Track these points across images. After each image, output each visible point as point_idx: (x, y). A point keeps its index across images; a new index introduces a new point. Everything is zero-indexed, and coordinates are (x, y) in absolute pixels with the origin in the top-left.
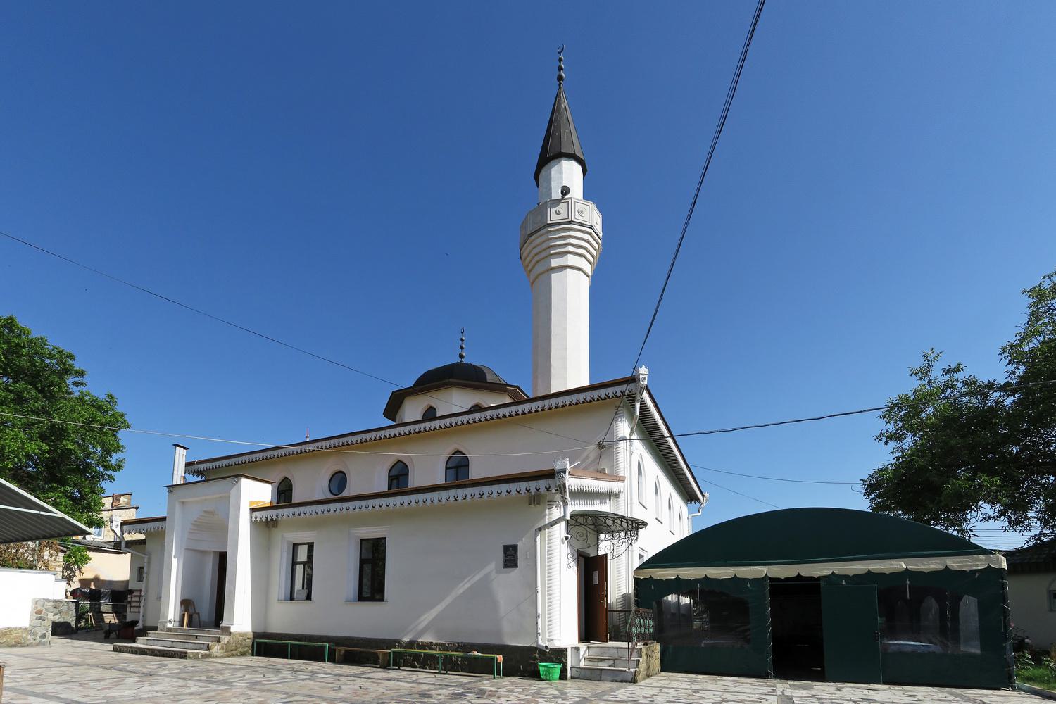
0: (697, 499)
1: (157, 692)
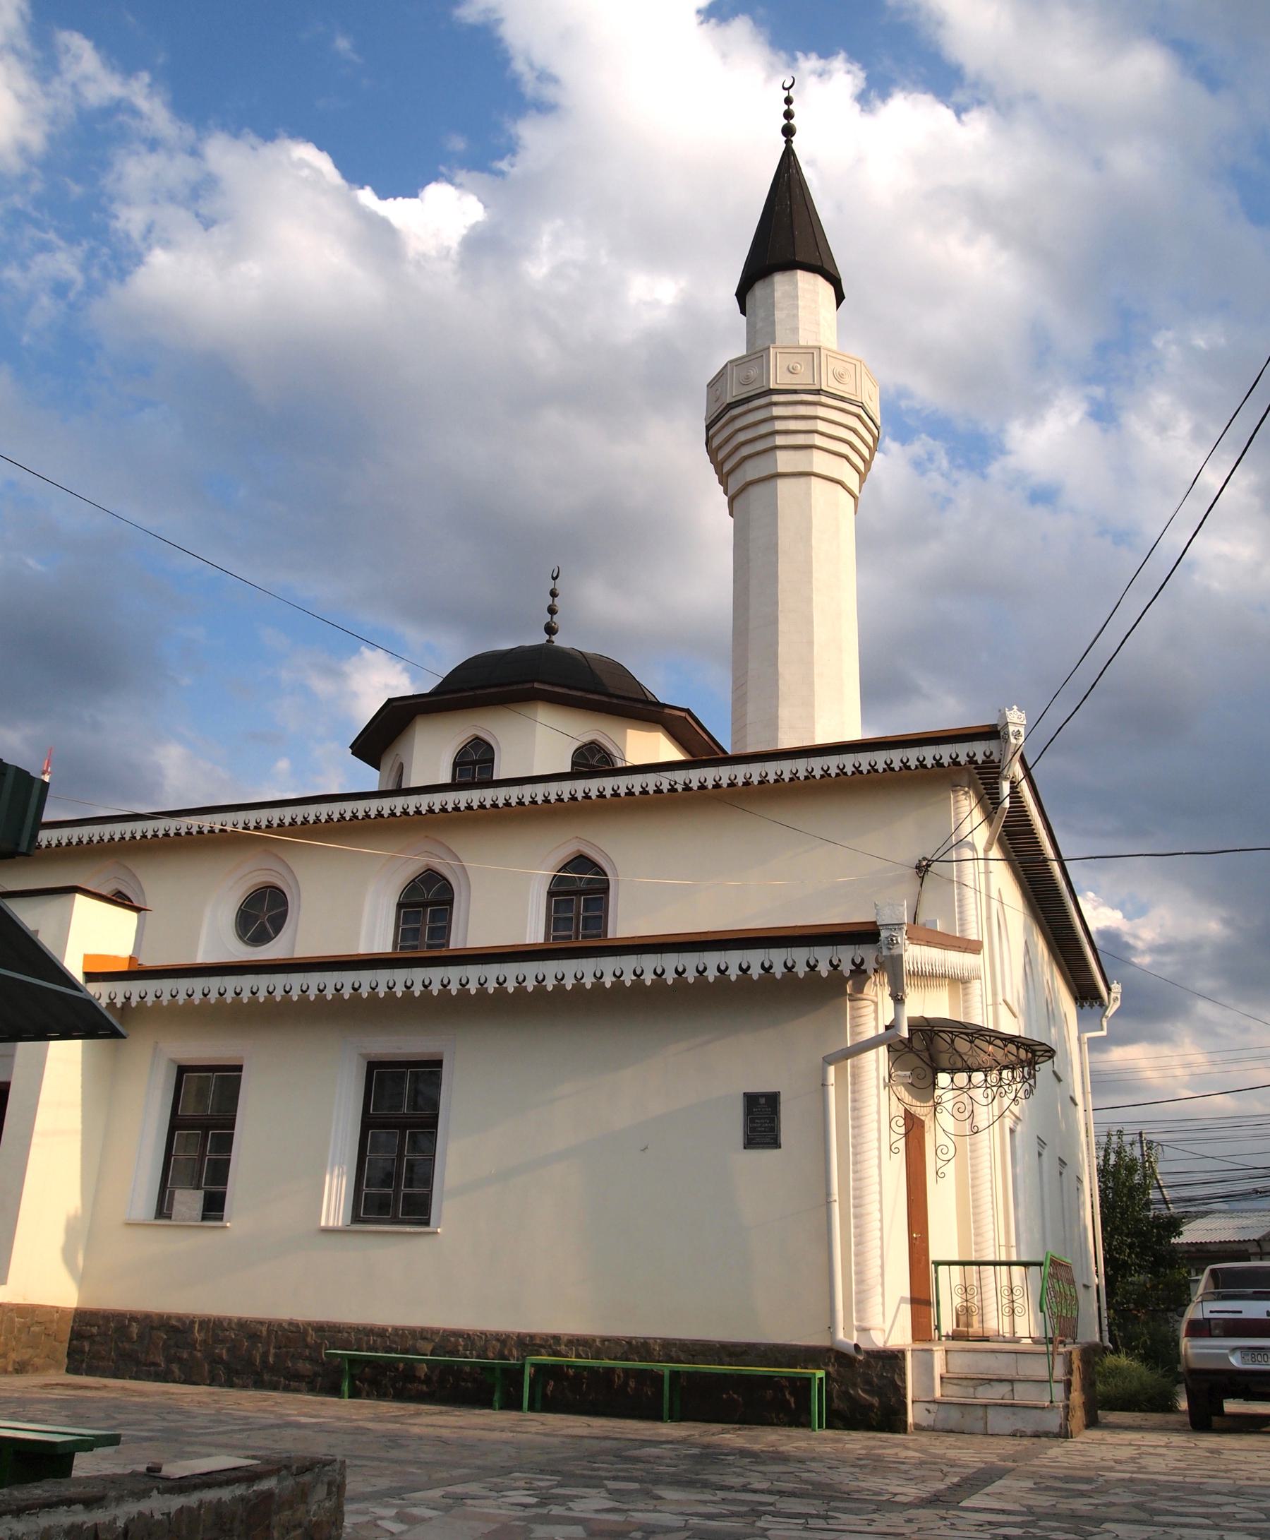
0: (1097, 997)
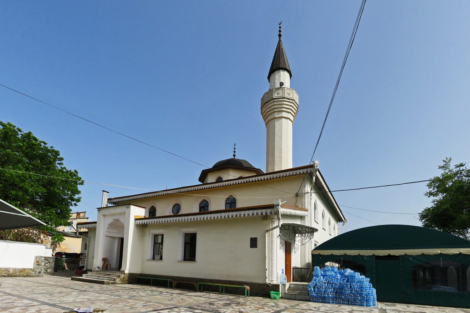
1: (85, 299)
